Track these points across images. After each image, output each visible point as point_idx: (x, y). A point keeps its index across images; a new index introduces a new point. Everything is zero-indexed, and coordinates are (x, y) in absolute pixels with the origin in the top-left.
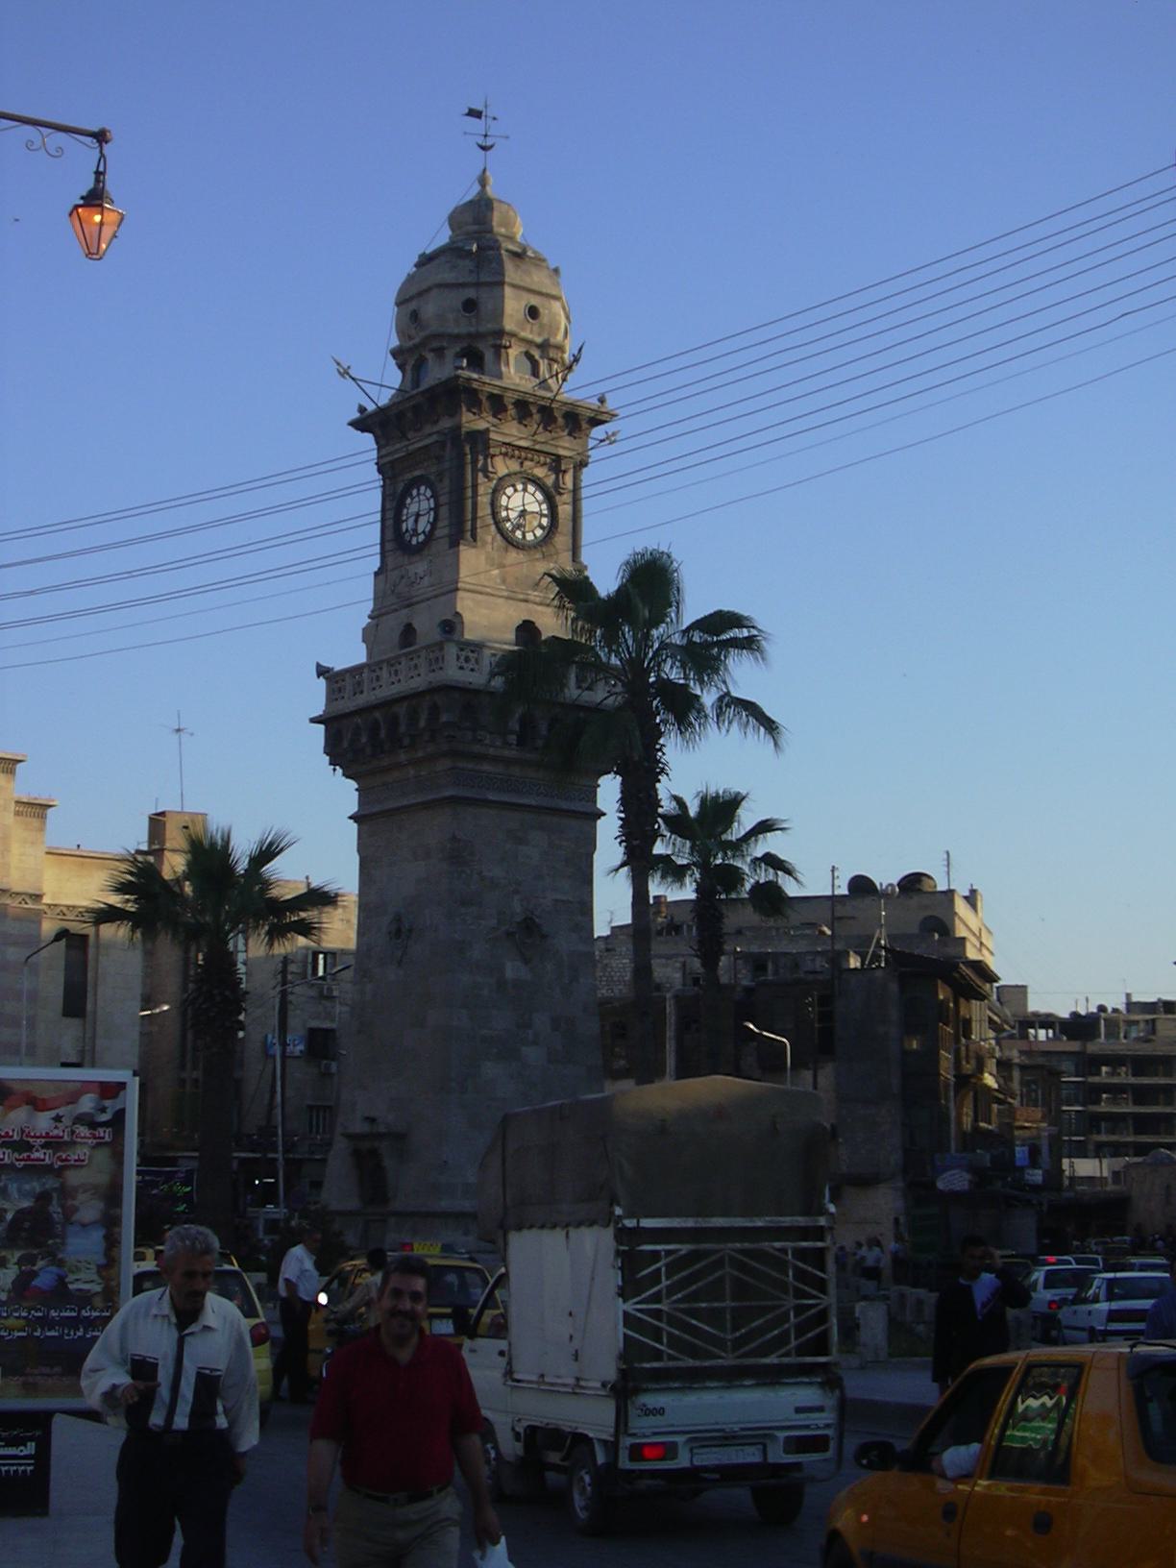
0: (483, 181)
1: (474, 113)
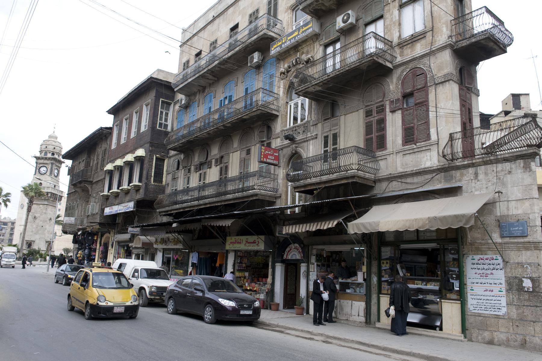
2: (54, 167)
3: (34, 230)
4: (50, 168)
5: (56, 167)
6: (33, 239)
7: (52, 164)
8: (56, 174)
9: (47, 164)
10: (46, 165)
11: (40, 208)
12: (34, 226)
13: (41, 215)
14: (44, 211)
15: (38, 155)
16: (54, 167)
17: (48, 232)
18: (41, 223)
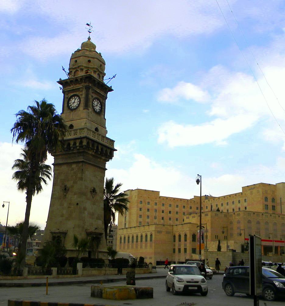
0: (89, 39)
1: (88, 25)
2: (92, 95)
3: (64, 212)
4: (84, 96)
5: (95, 96)
6: (63, 229)
7: (88, 88)
8: (98, 108)
9: (78, 90)
10: (77, 93)
11: (73, 169)
12: (65, 205)
13: (75, 182)
14: (79, 175)
15: (65, 77)
16: (92, 95)
17: (92, 215)
18: (196, 257)
